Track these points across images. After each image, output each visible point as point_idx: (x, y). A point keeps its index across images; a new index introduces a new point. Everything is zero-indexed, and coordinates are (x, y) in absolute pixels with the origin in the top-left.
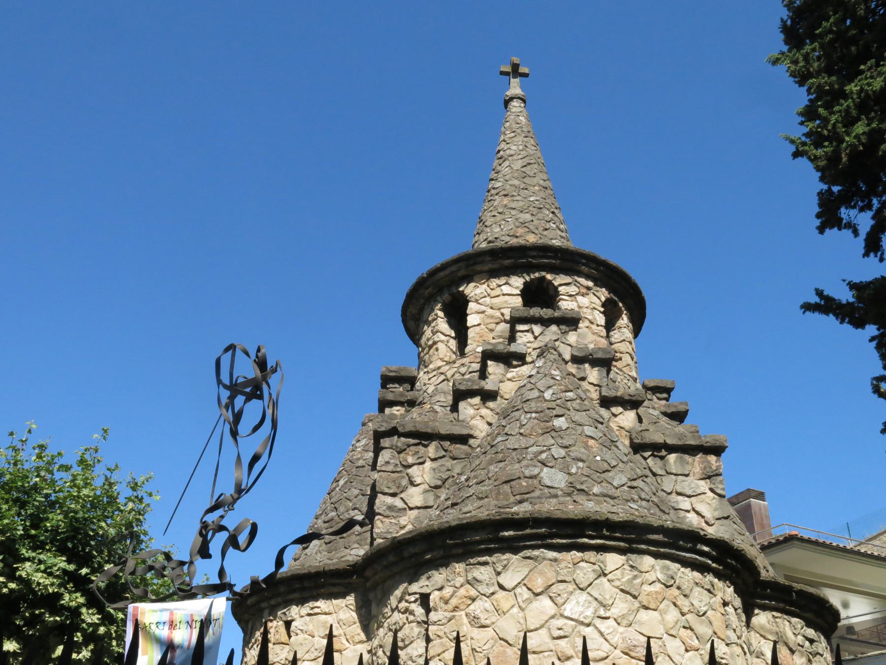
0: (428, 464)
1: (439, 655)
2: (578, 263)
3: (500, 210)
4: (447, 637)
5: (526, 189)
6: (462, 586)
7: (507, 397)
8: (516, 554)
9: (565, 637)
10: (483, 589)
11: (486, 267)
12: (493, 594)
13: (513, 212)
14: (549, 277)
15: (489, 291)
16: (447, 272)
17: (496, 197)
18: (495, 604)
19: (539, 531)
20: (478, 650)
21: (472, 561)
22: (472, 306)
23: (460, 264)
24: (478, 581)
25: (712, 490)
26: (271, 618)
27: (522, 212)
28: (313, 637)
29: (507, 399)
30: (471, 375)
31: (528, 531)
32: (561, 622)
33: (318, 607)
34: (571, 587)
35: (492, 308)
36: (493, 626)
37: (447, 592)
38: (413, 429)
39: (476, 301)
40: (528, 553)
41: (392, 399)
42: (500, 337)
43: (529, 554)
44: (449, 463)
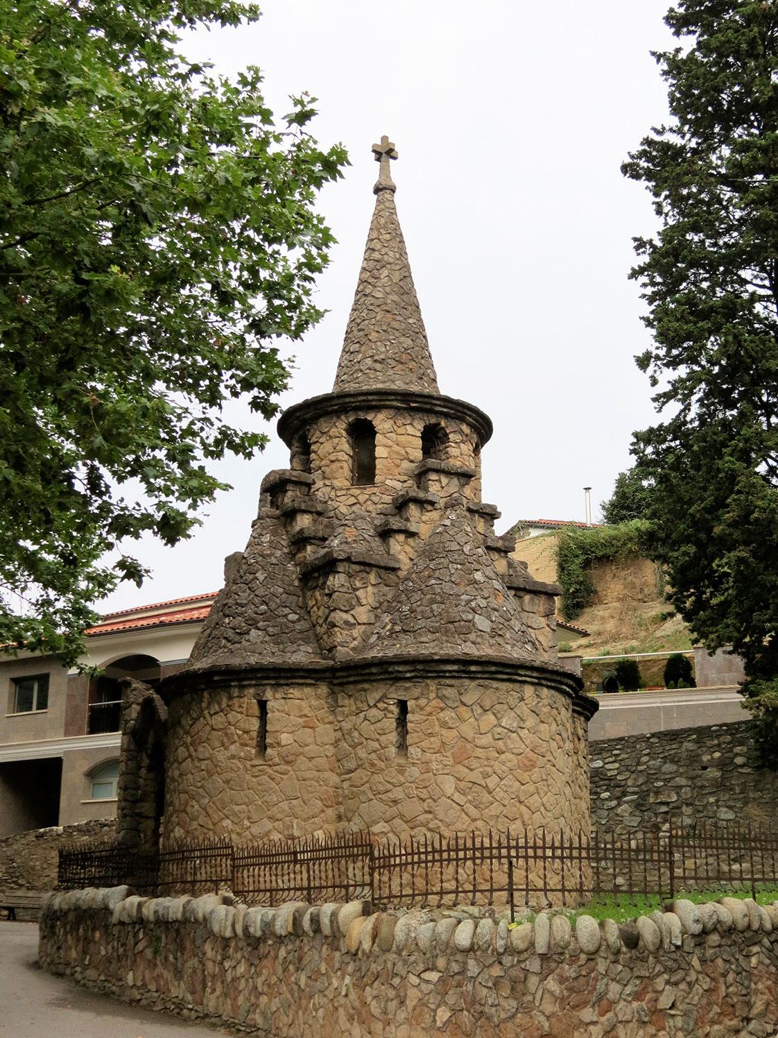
0: (370, 589)
3: (385, 328)
10: (450, 703)
17: (377, 310)
22: (378, 437)
25: (548, 625)
32: (499, 730)
34: (506, 707)
37: (423, 702)
42: (405, 474)
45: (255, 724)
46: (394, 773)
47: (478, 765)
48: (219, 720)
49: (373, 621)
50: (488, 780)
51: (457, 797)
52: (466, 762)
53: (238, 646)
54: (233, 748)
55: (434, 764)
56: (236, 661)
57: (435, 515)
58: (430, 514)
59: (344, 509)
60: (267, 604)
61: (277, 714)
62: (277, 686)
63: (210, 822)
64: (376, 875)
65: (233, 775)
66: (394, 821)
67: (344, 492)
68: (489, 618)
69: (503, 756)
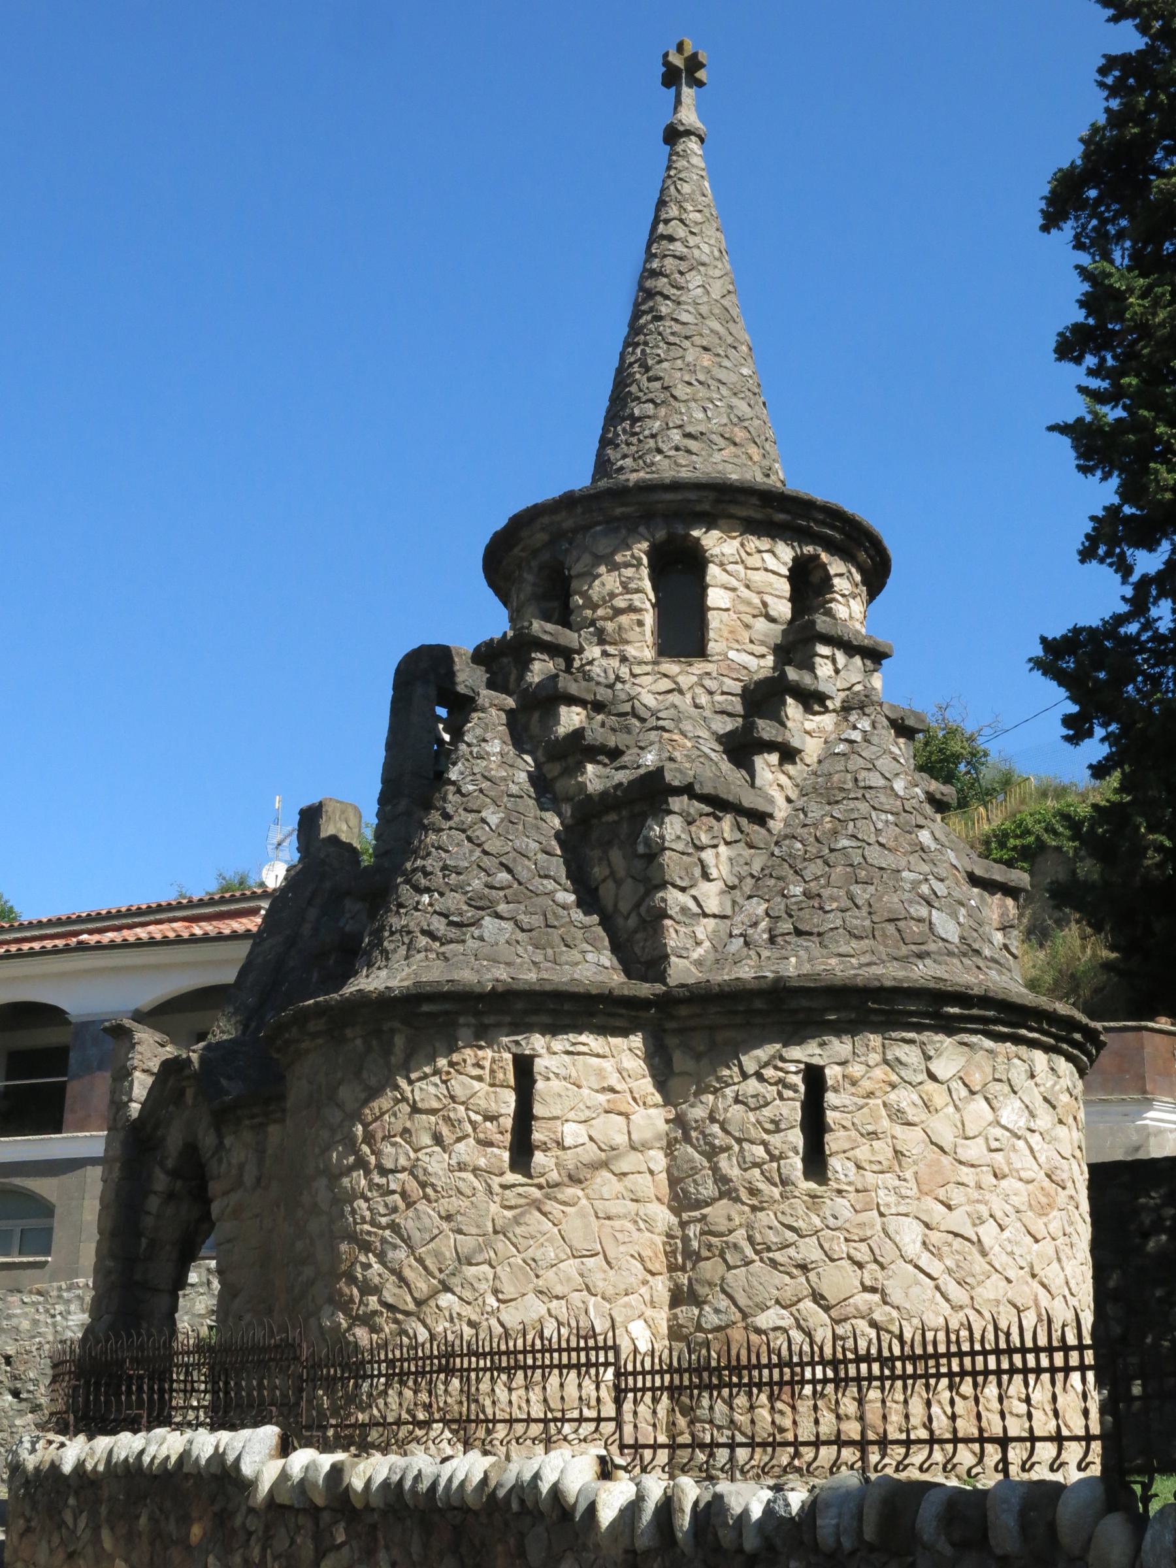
1: (844, 1152)
2: (860, 545)
3: (702, 377)
4: (857, 1130)
5: (735, 348)
6: (877, 1065)
7: (808, 761)
8: (949, 1036)
9: (1000, 1150)
10: (907, 1074)
11: (744, 513)
12: (920, 1083)
13: (724, 391)
14: (824, 557)
15: (743, 555)
16: (679, 496)
17: (686, 344)
18: (925, 1098)
19: (987, 1013)
20: (907, 1154)
21: (894, 1035)
22: (713, 570)
23: (705, 494)
24: (901, 1063)
26: (483, 1044)
27: (735, 394)
28: (579, 1087)
29: (808, 766)
30: (725, 697)
31: (975, 1012)
33: (584, 1044)
35: (748, 587)
36: (923, 1126)
37: (856, 1070)
38: (712, 791)
39: (722, 565)
40: (966, 1037)
41: (576, 694)
42: (763, 643)
43: (966, 1040)
44: (748, 852)
45: (507, 1102)
46: (801, 1209)
47: (963, 1200)
48: (427, 1091)
49: (729, 912)
50: (981, 1230)
51: (925, 1261)
52: (941, 1193)
53: (460, 948)
54: (466, 1150)
55: (881, 1193)
56: (467, 976)
57: (827, 721)
58: (817, 718)
59: (649, 700)
60: (509, 871)
61: (555, 1084)
62: (553, 1030)
63: (409, 1299)
64: (628, 1406)
65: (464, 1203)
66: (801, 1305)
67: (648, 668)
68: (954, 915)
69: (1004, 1183)
